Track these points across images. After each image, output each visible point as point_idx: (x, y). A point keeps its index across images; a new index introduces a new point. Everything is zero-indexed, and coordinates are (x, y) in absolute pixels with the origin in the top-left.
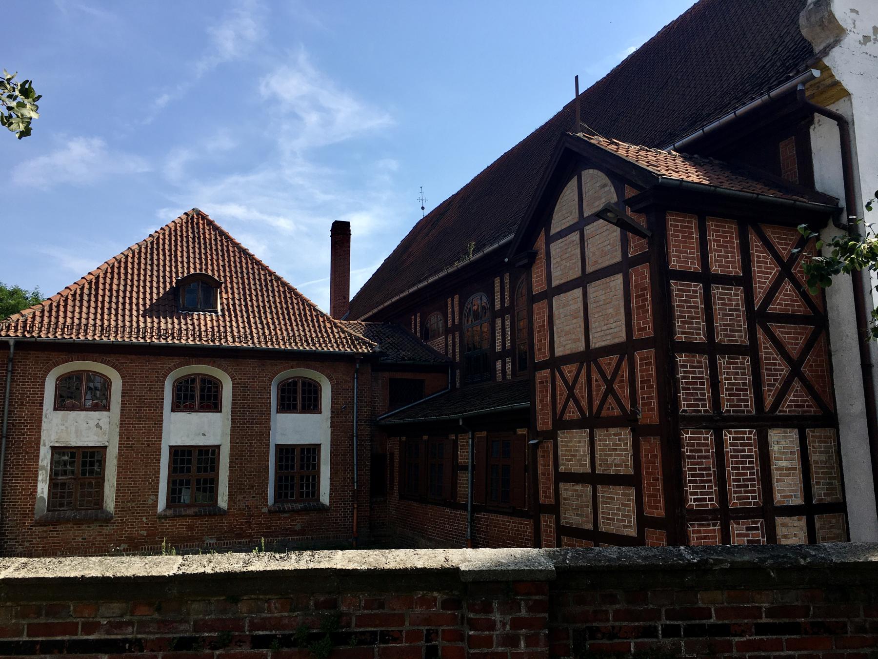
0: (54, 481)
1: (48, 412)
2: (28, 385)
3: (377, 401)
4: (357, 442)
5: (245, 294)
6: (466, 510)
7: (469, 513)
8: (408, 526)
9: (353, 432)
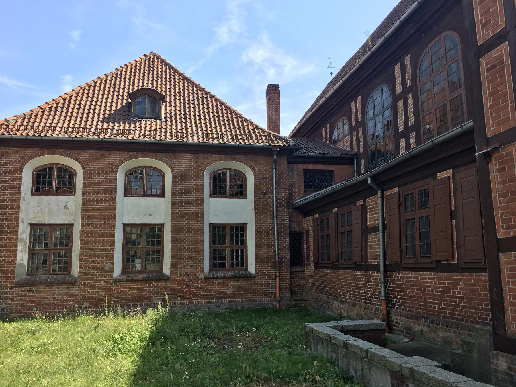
0: (32, 251)
1: (26, 195)
2: (9, 174)
3: (293, 188)
4: (277, 222)
5: (185, 107)
6: (379, 271)
7: (382, 273)
8: (322, 291)
9: (273, 213)
